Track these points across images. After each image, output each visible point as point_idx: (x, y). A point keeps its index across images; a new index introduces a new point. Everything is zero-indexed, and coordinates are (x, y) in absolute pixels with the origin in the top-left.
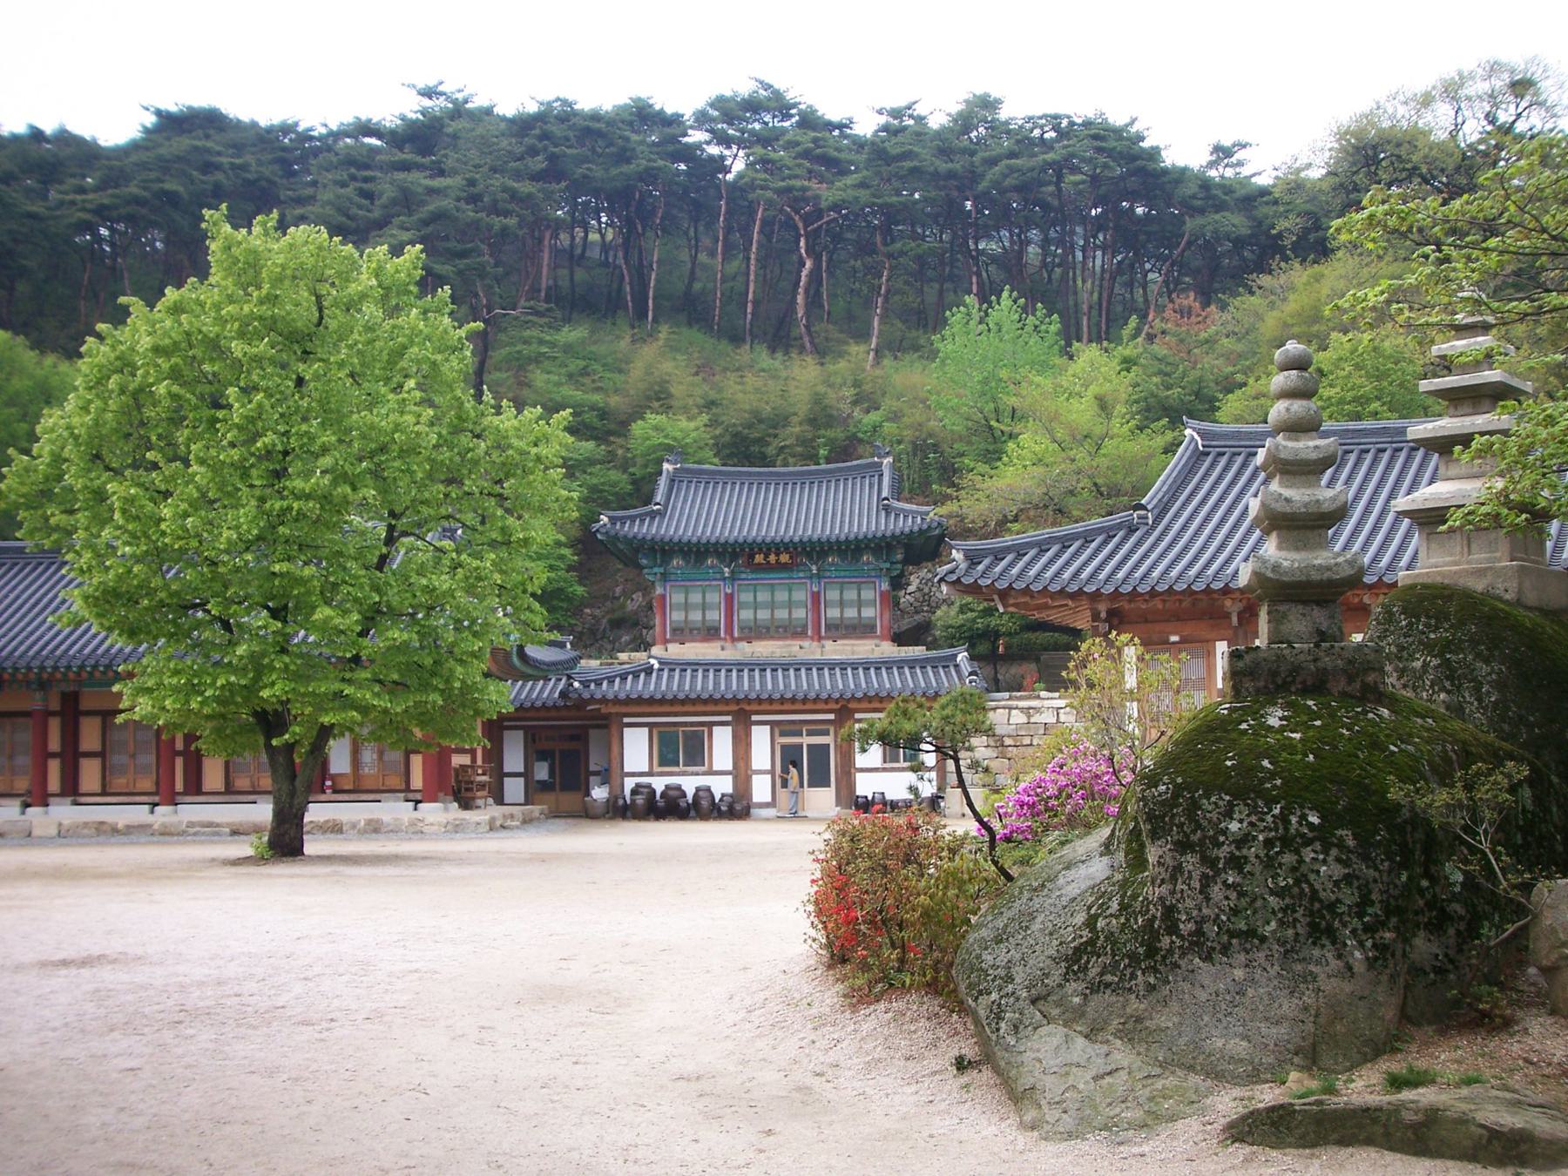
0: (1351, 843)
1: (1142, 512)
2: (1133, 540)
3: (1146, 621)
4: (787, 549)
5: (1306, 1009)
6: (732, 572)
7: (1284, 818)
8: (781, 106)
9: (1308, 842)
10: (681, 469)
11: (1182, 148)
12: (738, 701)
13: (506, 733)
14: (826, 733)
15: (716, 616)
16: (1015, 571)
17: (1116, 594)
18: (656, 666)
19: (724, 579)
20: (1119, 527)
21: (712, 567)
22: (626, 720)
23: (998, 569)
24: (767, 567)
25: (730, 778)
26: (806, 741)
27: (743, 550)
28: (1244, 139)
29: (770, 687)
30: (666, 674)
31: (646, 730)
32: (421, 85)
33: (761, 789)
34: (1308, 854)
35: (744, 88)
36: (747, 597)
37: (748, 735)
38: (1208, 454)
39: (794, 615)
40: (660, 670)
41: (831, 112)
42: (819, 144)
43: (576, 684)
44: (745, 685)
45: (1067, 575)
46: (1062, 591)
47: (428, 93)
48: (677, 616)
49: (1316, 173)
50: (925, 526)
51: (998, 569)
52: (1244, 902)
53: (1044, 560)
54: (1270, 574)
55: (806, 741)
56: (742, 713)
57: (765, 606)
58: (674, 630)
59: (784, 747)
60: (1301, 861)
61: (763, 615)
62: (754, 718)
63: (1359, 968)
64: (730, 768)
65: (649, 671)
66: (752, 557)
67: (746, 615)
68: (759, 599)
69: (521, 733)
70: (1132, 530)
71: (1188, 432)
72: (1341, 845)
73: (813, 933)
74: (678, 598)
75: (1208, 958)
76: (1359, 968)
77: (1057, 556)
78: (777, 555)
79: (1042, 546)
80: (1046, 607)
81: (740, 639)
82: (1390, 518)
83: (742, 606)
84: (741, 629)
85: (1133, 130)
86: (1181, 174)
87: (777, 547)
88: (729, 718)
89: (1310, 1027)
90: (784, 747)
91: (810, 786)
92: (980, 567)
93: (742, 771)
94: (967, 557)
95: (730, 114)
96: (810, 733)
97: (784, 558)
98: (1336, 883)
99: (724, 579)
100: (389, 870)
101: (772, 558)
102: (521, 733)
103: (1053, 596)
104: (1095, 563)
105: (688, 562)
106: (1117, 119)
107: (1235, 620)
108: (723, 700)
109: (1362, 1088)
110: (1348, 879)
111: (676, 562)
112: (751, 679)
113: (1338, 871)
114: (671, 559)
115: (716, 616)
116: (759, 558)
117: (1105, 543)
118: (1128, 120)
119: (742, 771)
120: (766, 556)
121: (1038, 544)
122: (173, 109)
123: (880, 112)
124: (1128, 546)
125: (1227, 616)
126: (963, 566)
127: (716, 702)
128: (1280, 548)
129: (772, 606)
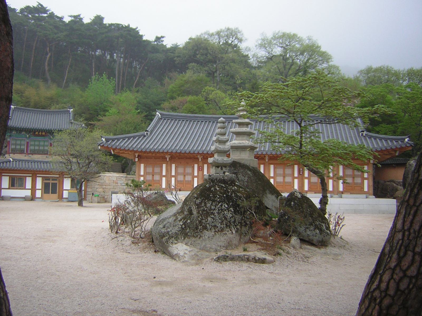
0: (233, 211)
1: (147, 132)
3: (147, 158)
4: (44, 131)
5: (225, 239)
6: (29, 136)
7: (221, 206)
9: (226, 210)
10: (16, 107)
11: (148, 35)
12: (34, 171)
14: (56, 180)
15: (24, 147)
16: (117, 144)
17: (141, 151)
18: (12, 160)
19: (27, 138)
20: (142, 135)
21: (24, 134)
22: (3, 174)
23: (113, 143)
24: (38, 135)
25: (30, 191)
26: (51, 182)
27: (33, 131)
28: (163, 36)
29: (14, 166)
30: (14, 163)
31: (8, 177)
33: (39, 194)
34: (226, 212)
36: (32, 143)
37: (36, 179)
38: (162, 119)
39: (36, 148)
40: (13, 161)
41: (58, 13)
44: (35, 167)
45: (130, 146)
46: (129, 149)
48: (13, 147)
49: (181, 46)
51: (113, 143)
52: (214, 220)
53: (124, 142)
54: (216, 161)
55: (51, 182)
56: (34, 174)
57: (42, 146)
58: (12, 150)
59: (45, 183)
60: (224, 214)
61: (37, 148)
62: (38, 175)
63: (234, 232)
64: (30, 188)
65: (10, 161)
66: (35, 132)
67: (32, 148)
68: (36, 144)
70: (145, 136)
71: (157, 113)
72: (231, 211)
74: (13, 142)
75: (208, 231)
76: (234, 232)
77: (127, 141)
78: (42, 132)
79: (124, 139)
80: (123, 153)
81: (30, 154)
82: (212, 141)
83: (31, 145)
84: (30, 151)
85: (137, 29)
86: (148, 42)
87: (42, 131)
88: (31, 175)
89: (225, 242)
90: (45, 183)
91: (52, 193)
92: (109, 143)
93: (34, 189)
94: (106, 140)
96: (53, 180)
97: (44, 133)
98: (230, 218)
99: (27, 138)
100: (16, 199)
101: (40, 133)
103: (126, 151)
104: (137, 143)
105: (17, 133)
106: (133, 26)
107: (168, 160)
108: (31, 171)
109: (238, 252)
110: (232, 217)
111: (14, 132)
112: (22, 164)
113: (231, 215)
114: (22, 132)
115: (24, 147)
116: (37, 133)
117: (138, 139)
119: (34, 189)
120: (39, 132)
121: (123, 138)
123: (71, 16)
124: (144, 140)
125: (166, 158)
126: (105, 142)
127: (28, 171)
128: (217, 156)
129: (39, 146)
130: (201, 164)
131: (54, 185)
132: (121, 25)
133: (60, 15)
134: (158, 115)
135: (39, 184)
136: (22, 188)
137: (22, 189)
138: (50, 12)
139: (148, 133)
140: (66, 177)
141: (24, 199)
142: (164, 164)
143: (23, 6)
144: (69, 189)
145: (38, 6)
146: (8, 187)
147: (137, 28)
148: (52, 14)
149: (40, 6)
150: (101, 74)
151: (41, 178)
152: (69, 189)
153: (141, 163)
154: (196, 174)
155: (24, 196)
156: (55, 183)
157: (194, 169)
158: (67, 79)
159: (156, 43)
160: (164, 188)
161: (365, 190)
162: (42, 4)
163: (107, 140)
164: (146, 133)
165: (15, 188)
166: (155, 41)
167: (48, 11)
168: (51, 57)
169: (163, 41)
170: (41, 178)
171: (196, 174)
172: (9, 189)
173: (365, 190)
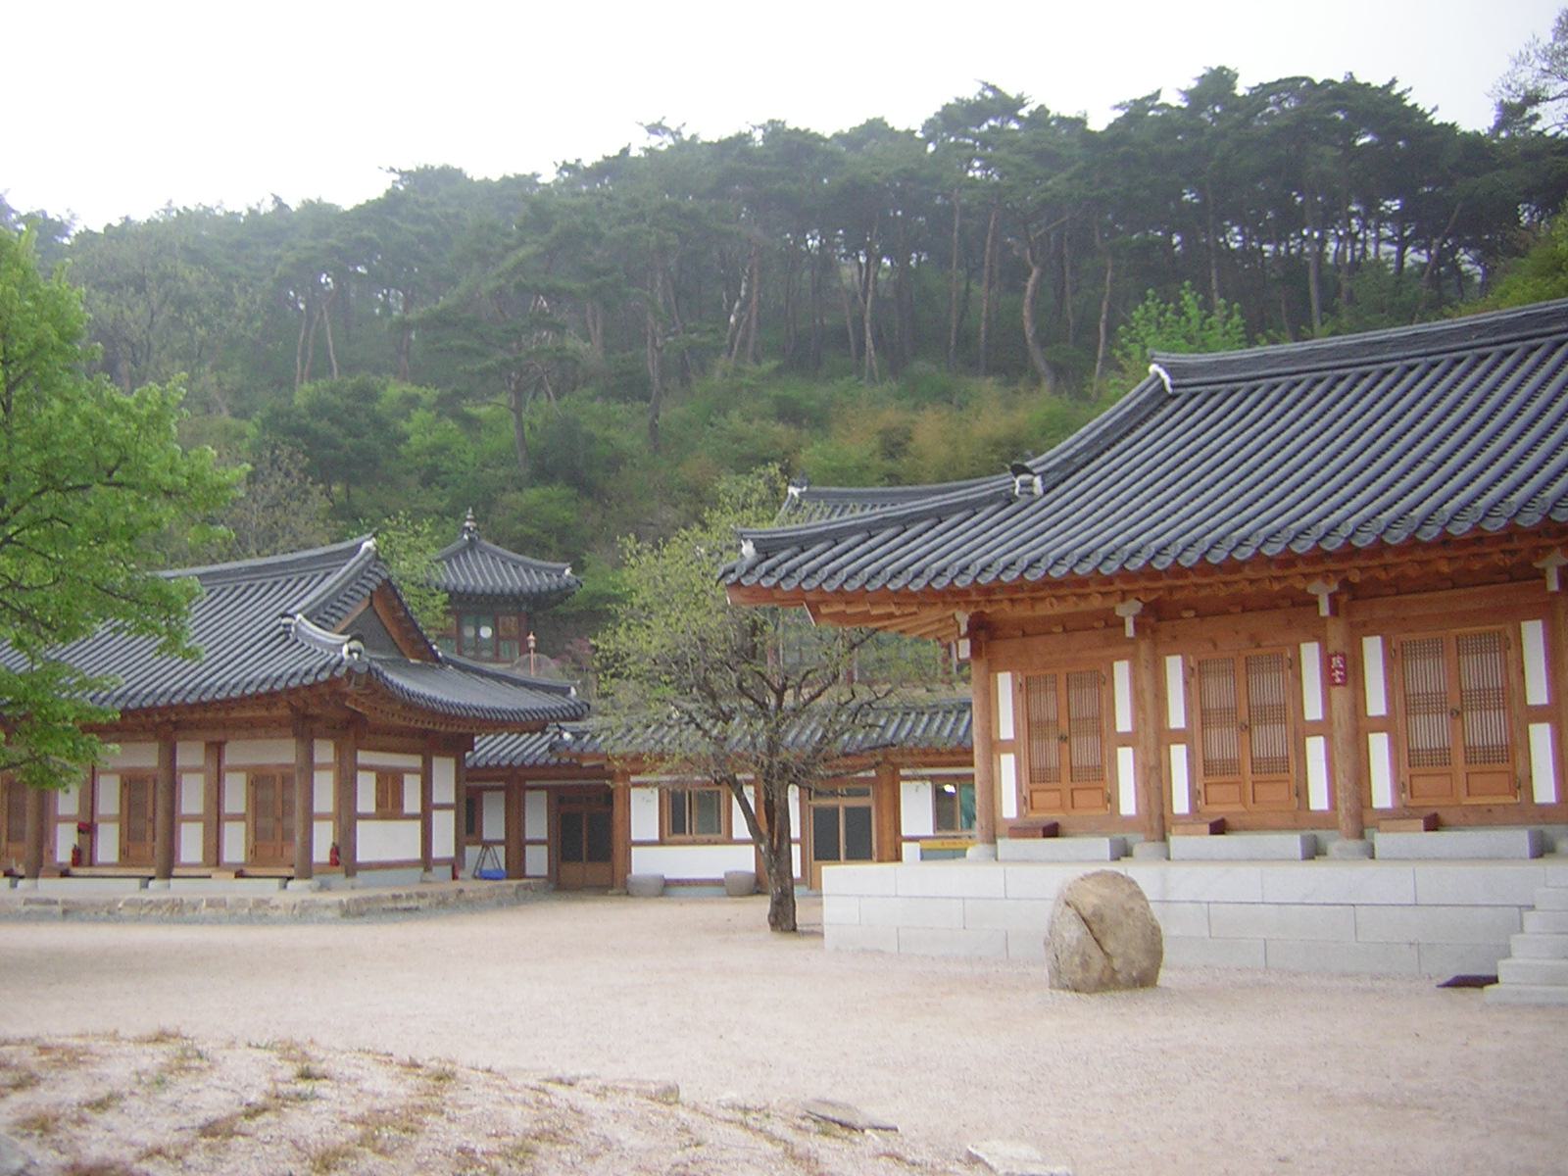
2: (1009, 509)
8: (1007, 106)
13: (529, 795)
22: (528, 783)
32: (647, 123)
35: (971, 92)
41: (1062, 106)
42: (1053, 140)
43: (567, 736)
46: (840, 591)
47: (655, 129)
50: (563, 584)
55: (843, 803)
69: (544, 793)
73: (324, 1066)
85: (1395, 92)
88: (502, 784)
95: (956, 118)
100: (697, 889)
102: (544, 793)
118: (1386, 82)
122: (1194, 84)
130: (1337, 638)
131: (859, 820)
132: (1303, 79)
133: (1070, 112)
134: (1158, 376)
135: (537, 824)
136: (713, 837)
137: (716, 843)
138: (1033, 107)
139: (1030, 484)
140: (907, 778)
141: (722, 890)
142: (1120, 659)
143: (931, 109)
144: (930, 833)
145: (981, 95)
146: (656, 837)
147: (1393, 82)
148: (1042, 110)
149: (989, 94)
150: (1170, 297)
151: (545, 793)
152: (930, 833)
153: (993, 668)
154: (1313, 711)
155: (721, 876)
156: (859, 809)
157: (1298, 677)
158: (1095, 361)
159: (1503, 134)
160: (1128, 819)
161: (1539, 799)
162: (991, 83)
163: (765, 549)
164: (1023, 485)
165: (688, 837)
166: (1501, 125)
167: (1020, 102)
168: (1039, 280)
169: (1536, 118)
170: (545, 793)
171: (1313, 711)
172: (661, 842)
173: (1539, 799)
